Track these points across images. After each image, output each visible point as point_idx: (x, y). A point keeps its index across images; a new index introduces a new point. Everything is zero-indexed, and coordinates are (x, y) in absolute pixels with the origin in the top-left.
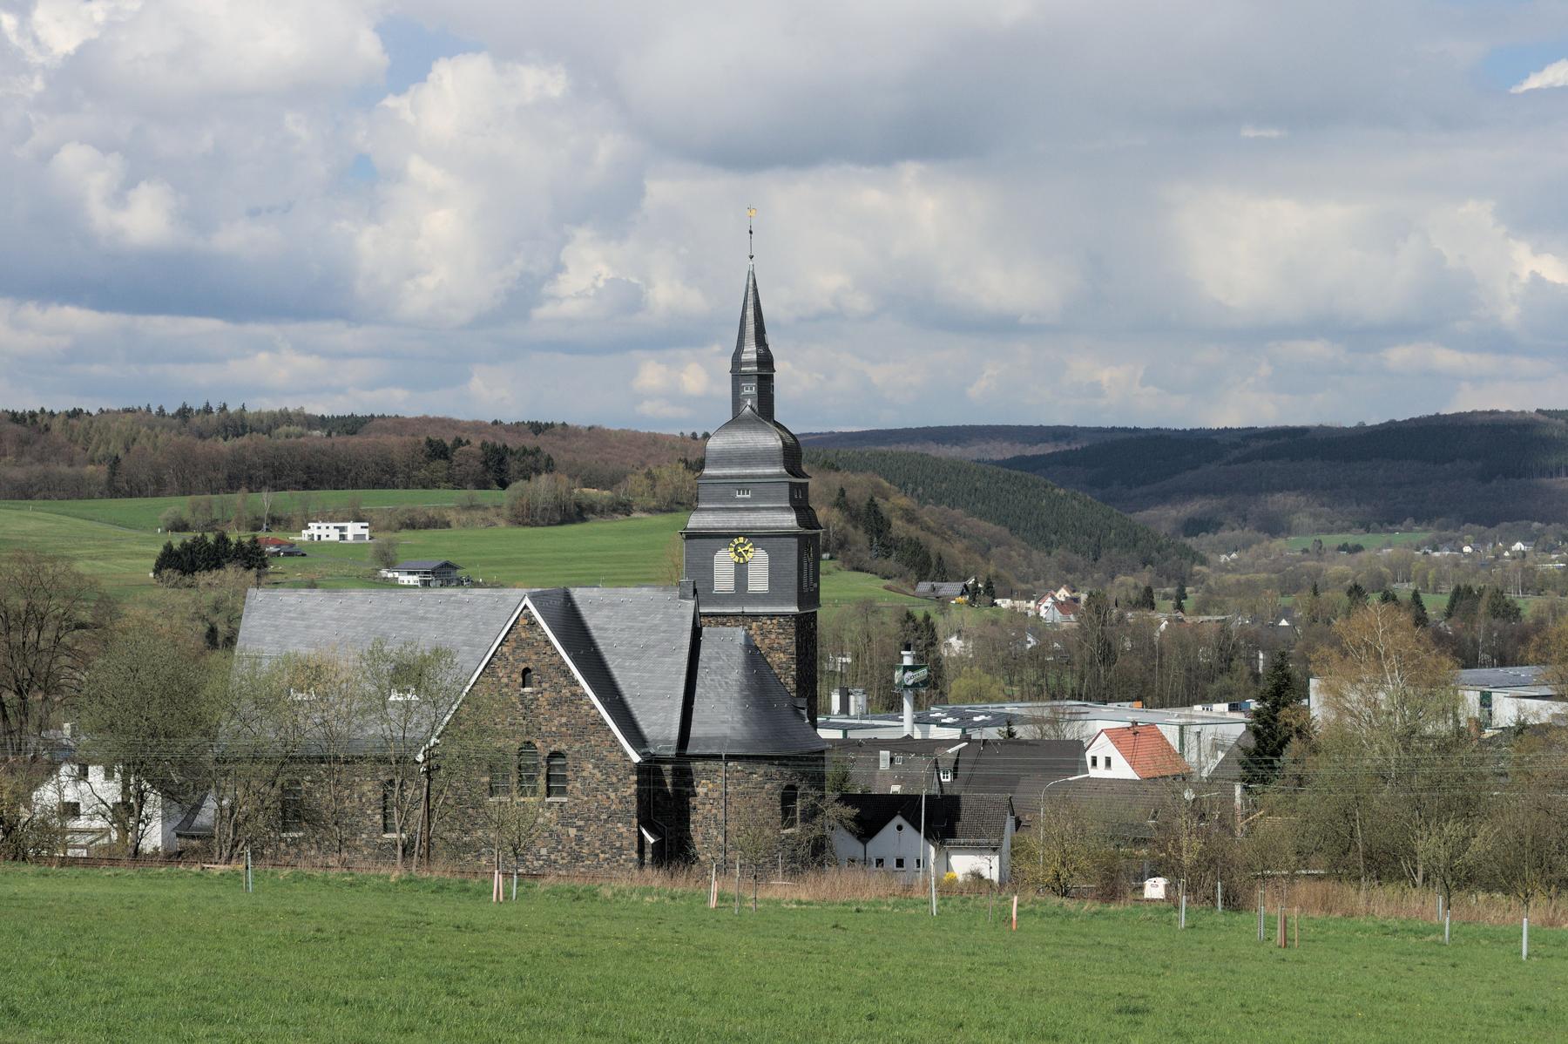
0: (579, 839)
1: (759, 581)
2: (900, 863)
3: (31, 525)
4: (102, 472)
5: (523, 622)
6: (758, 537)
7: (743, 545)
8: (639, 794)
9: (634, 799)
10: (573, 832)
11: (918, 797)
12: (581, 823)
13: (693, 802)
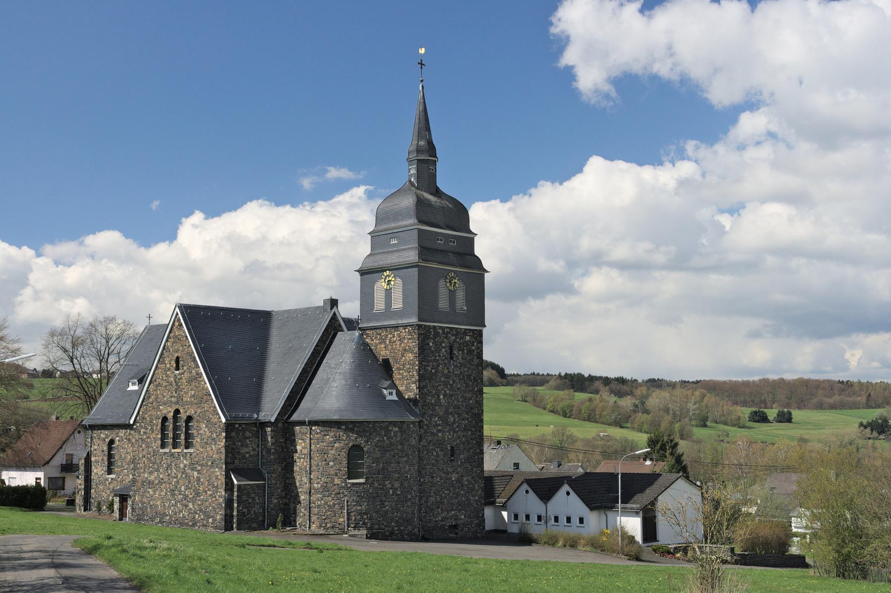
0: (198, 479)
1: (397, 304)
2: (569, 520)
3: (823, 418)
4: (864, 399)
5: (177, 324)
6: (395, 269)
7: (388, 276)
8: (226, 447)
9: (223, 450)
10: (196, 474)
11: (614, 476)
12: (199, 468)
13: (296, 456)
